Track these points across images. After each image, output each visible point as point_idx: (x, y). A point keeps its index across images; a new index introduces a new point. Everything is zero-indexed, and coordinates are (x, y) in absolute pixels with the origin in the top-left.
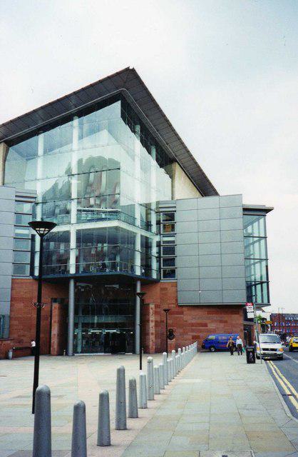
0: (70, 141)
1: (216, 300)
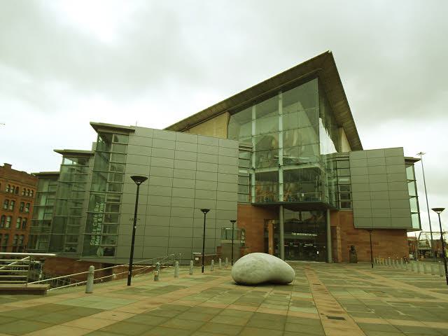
0: (277, 109)
1: (387, 225)
